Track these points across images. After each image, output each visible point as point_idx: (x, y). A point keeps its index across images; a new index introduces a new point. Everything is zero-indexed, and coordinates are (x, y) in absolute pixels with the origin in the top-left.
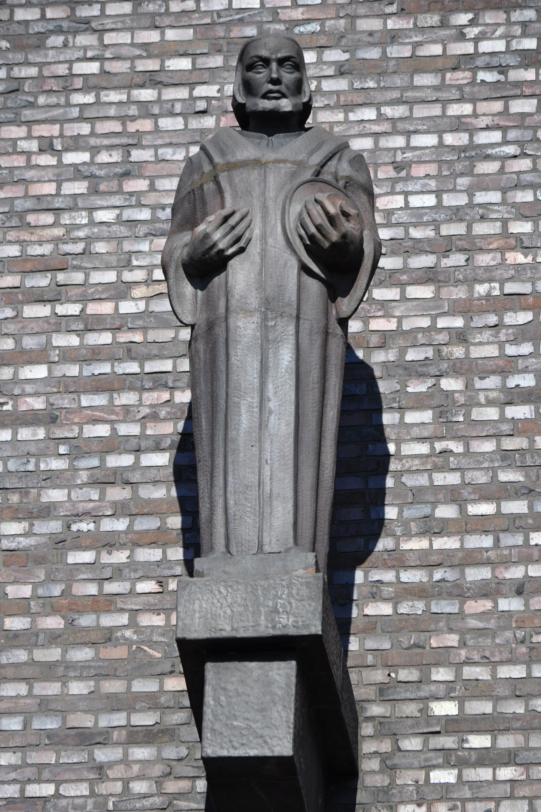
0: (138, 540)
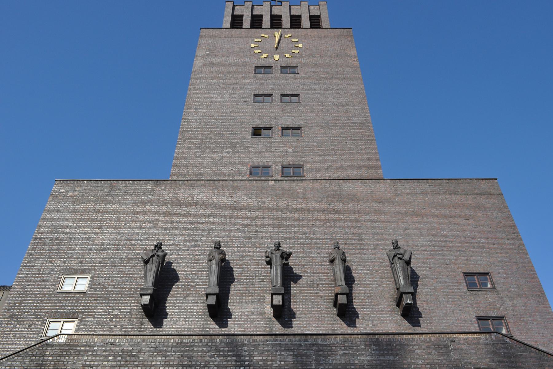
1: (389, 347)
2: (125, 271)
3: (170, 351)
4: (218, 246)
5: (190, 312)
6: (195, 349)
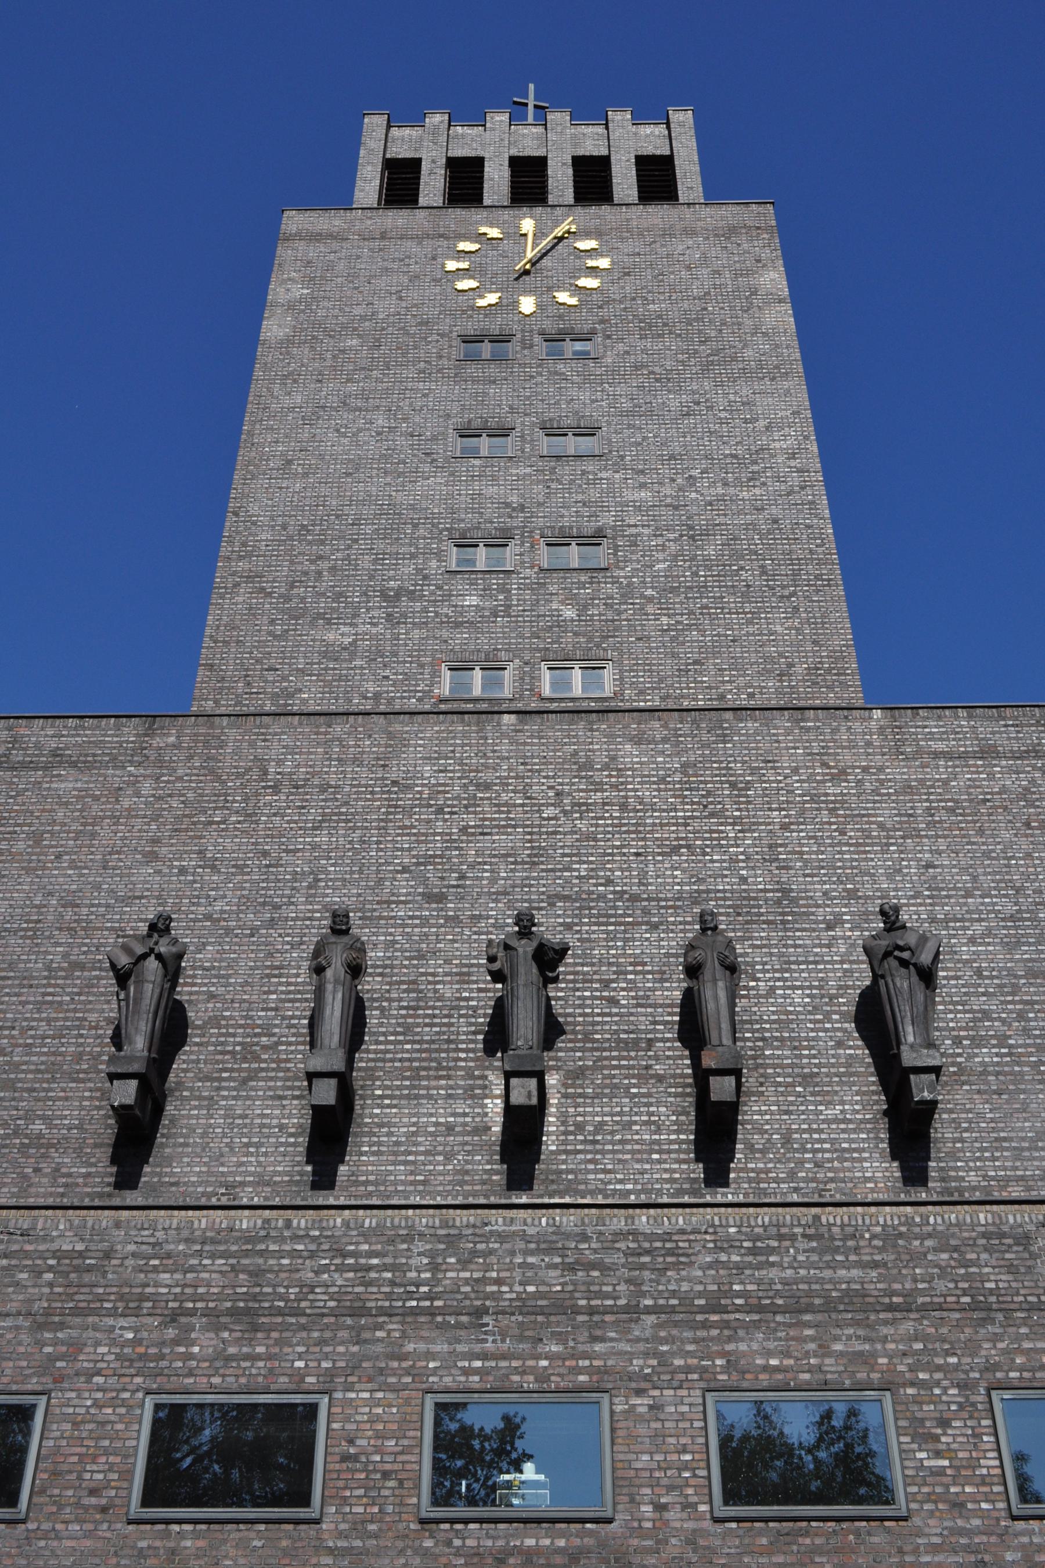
0: (298, 1043)
2: (61, 1003)
3: (199, 1254)
5: (262, 1126)
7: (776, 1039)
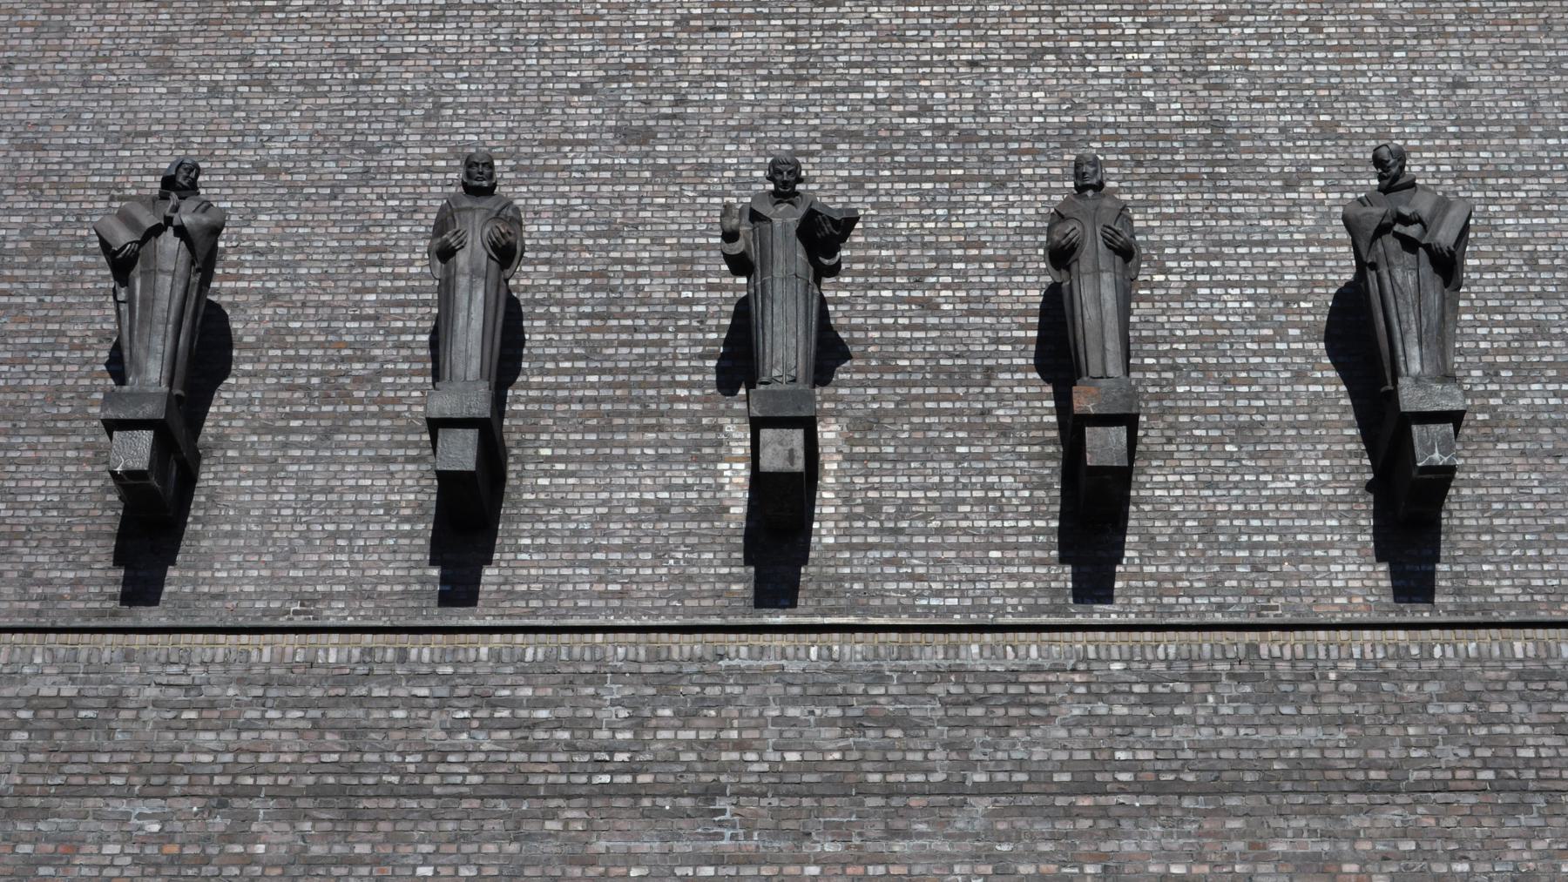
1: (1305, 687)
2: (21, 307)
4: (478, 180)
5: (358, 505)
6: (377, 692)
7: (1196, 367)
